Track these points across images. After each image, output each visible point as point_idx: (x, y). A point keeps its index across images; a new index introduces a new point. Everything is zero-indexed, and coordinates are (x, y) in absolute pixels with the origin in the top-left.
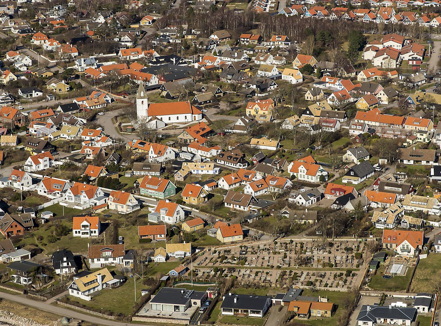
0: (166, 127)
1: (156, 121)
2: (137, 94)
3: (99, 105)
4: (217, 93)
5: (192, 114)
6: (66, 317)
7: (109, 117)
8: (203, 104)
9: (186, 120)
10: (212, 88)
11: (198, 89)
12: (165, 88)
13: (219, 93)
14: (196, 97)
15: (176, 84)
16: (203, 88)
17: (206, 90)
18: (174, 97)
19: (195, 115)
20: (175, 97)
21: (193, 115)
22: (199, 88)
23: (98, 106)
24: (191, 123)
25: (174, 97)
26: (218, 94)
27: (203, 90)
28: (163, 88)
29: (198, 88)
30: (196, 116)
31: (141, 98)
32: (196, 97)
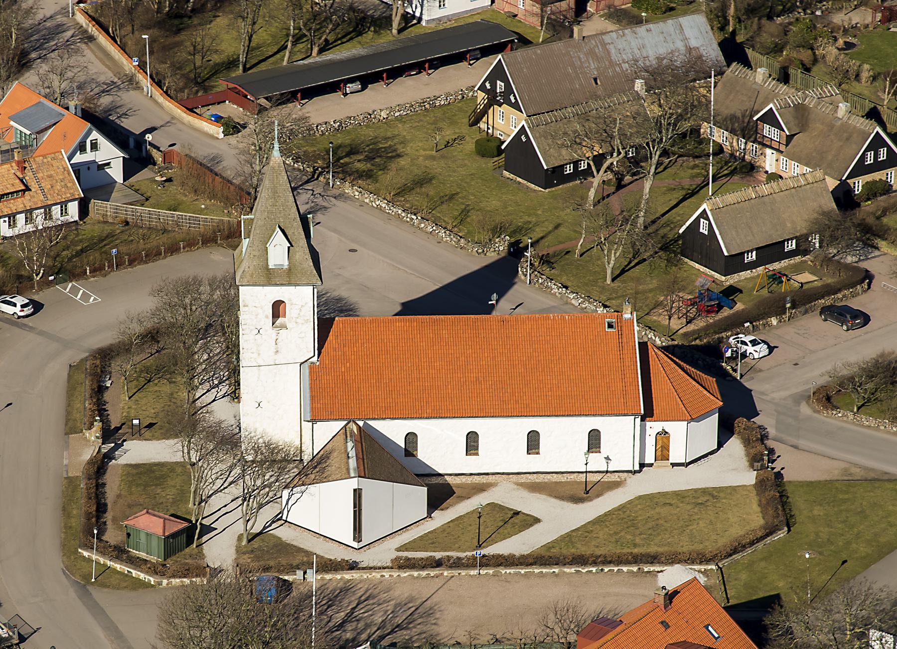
0: (441, 518)
1: (357, 493)
2: (245, 242)
3: (29, 214)
4: (861, 169)
5: (648, 414)
6: (538, 44)
7: (67, 344)
8: (752, 265)
9: (597, 462)
10: (831, 127)
11: (733, 118)
12: (508, 90)
13: (878, 166)
14: (704, 215)
15: (592, 53)
16: (769, 118)
17: (790, 138)
18: (562, 167)
19: (669, 426)
20: (569, 170)
21: (654, 427)
22: (748, 105)
23: (21, 218)
24: (637, 487)
25: (562, 167)
26: (868, 178)
27: (768, 130)
28: (500, 85)
29: (735, 106)
30: (677, 430)
31: (269, 277)
32: (704, 215)
